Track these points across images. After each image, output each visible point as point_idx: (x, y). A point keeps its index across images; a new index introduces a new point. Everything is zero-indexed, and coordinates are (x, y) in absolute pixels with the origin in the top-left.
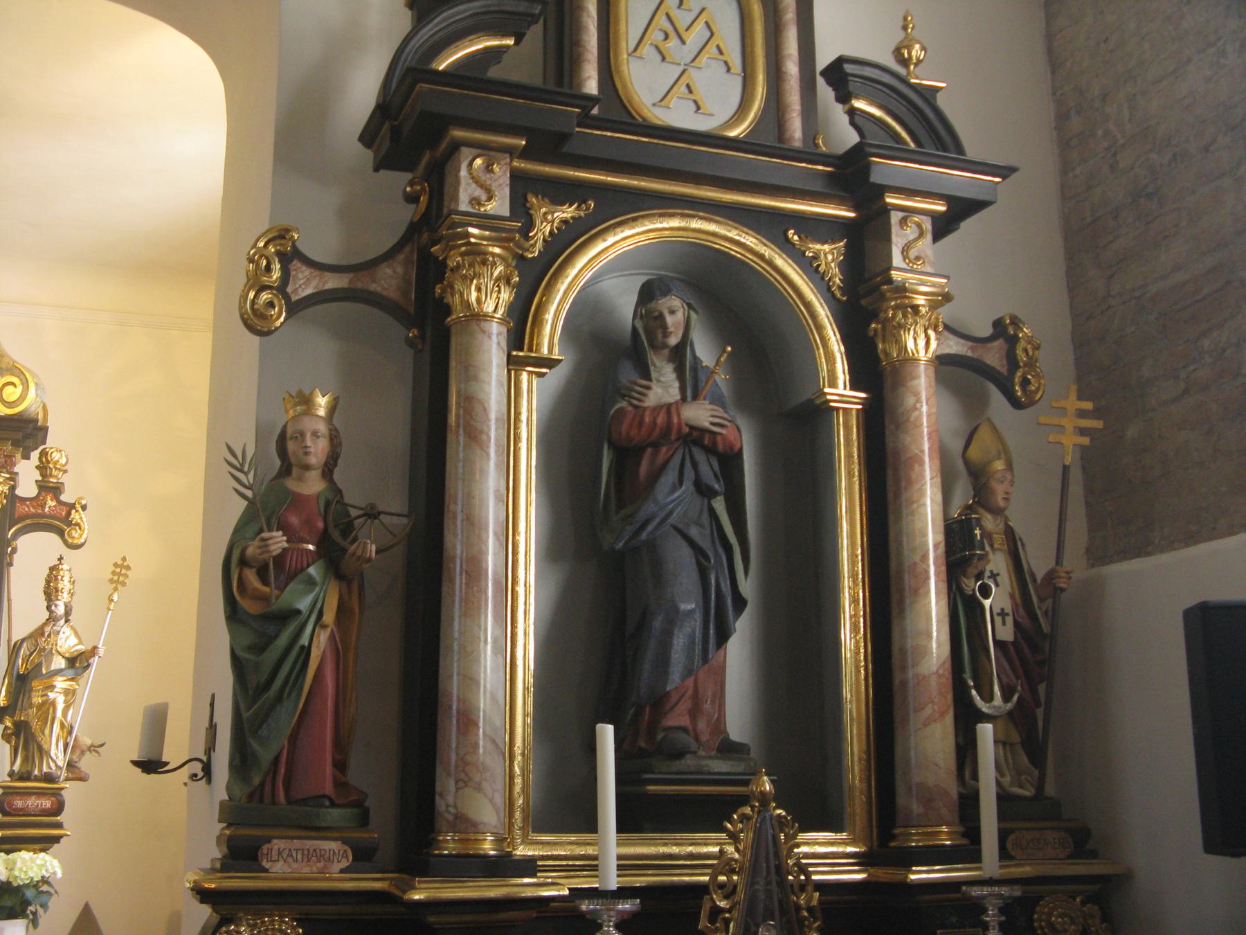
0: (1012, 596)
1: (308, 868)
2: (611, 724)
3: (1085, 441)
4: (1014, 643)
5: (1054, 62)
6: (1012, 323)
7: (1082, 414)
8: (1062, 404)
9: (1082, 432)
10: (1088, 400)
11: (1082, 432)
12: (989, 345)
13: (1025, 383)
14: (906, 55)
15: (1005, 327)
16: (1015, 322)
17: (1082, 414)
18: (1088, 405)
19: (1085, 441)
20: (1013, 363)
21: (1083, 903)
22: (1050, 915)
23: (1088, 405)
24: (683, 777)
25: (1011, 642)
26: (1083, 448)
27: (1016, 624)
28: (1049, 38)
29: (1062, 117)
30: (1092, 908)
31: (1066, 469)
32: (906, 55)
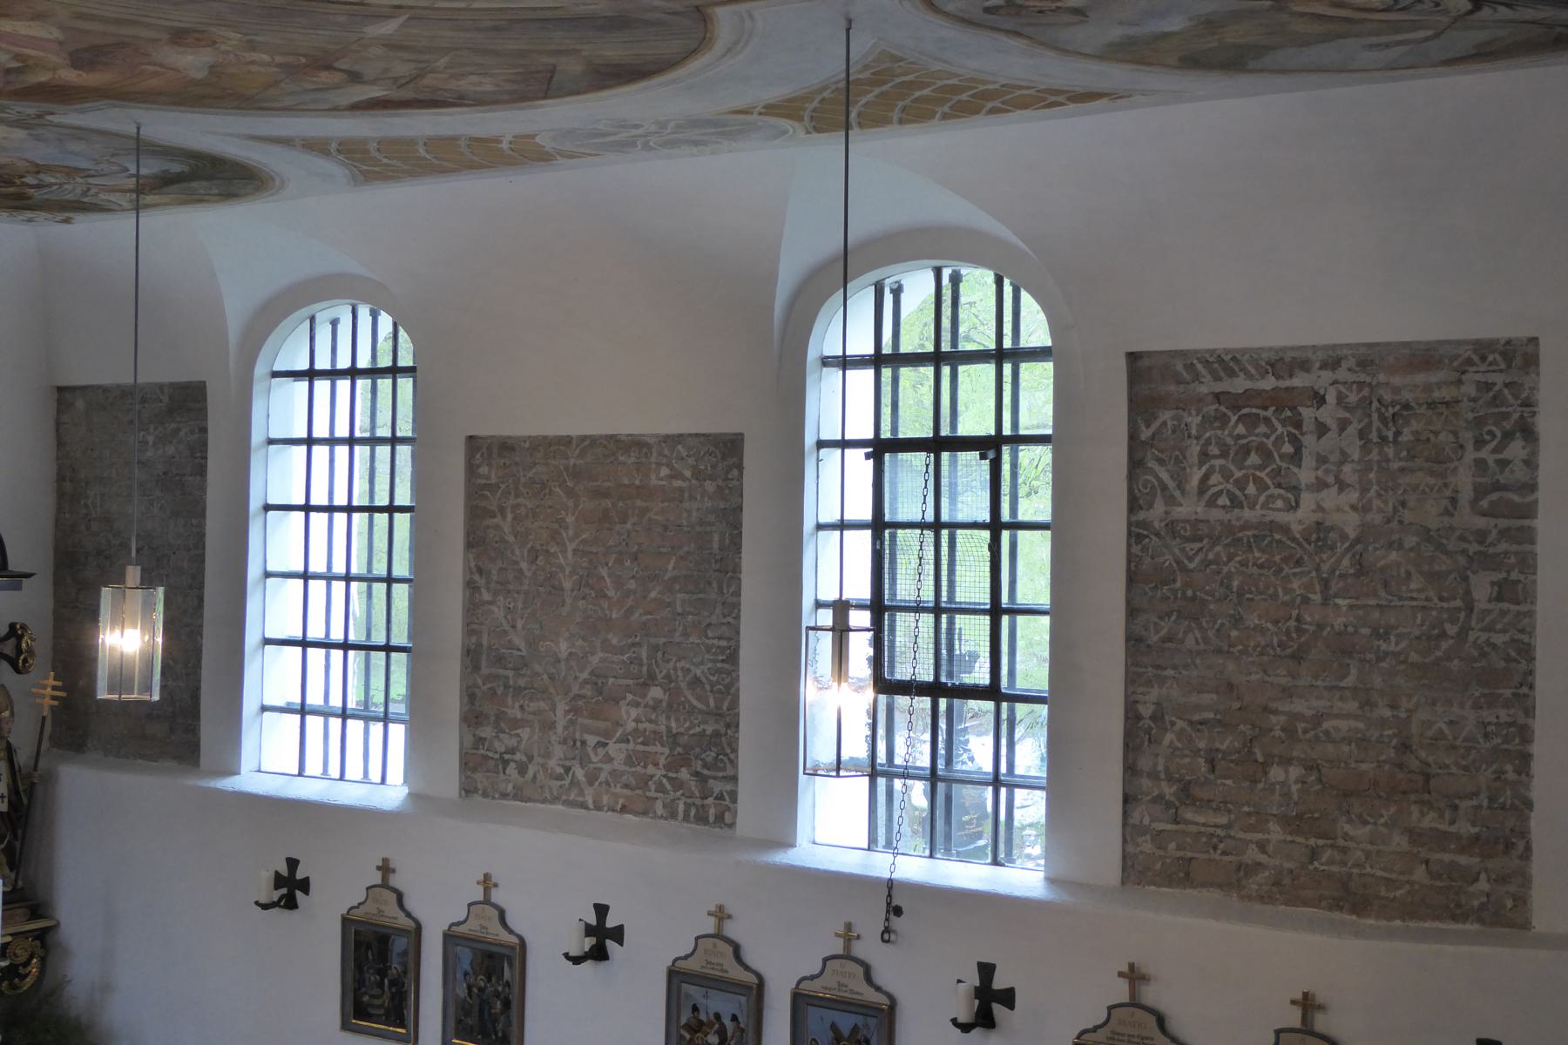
0: (8, 785)
1: (659, 653)
2: (1001, 618)
3: (56, 703)
4: (8, 813)
5: (60, 443)
6: (21, 627)
7: (54, 688)
8: (45, 682)
9: (54, 698)
10: (59, 681)
11: (54, 698)
12: (6, 642)
13: (25, 661)
14: (284, 901)
15: (16, 631)
16: (24, 627)
17: (54, 688)
18: (59, 683)
19: (56, 703)
20: (19, 651)
21: (32, 941)
22: (15, 949)
23: (59, 683)
24: (887, 561)
25: (6, 812)
26: (52, 707)
27: (9, 801)
28: (58, 425)
29: (61, 478)
30: (38, 943)
31: (44, 718)
32: (284, 901)
